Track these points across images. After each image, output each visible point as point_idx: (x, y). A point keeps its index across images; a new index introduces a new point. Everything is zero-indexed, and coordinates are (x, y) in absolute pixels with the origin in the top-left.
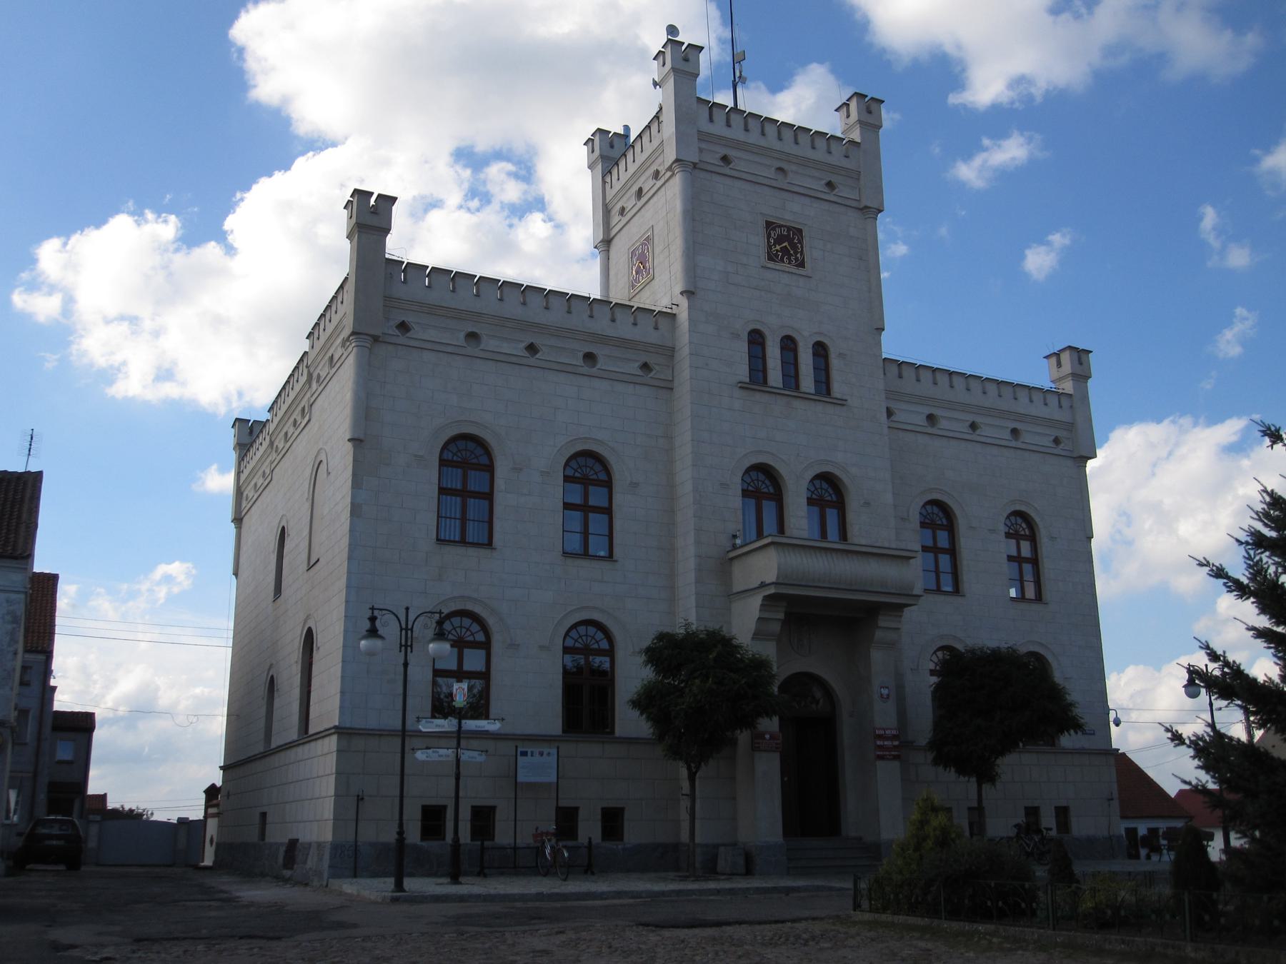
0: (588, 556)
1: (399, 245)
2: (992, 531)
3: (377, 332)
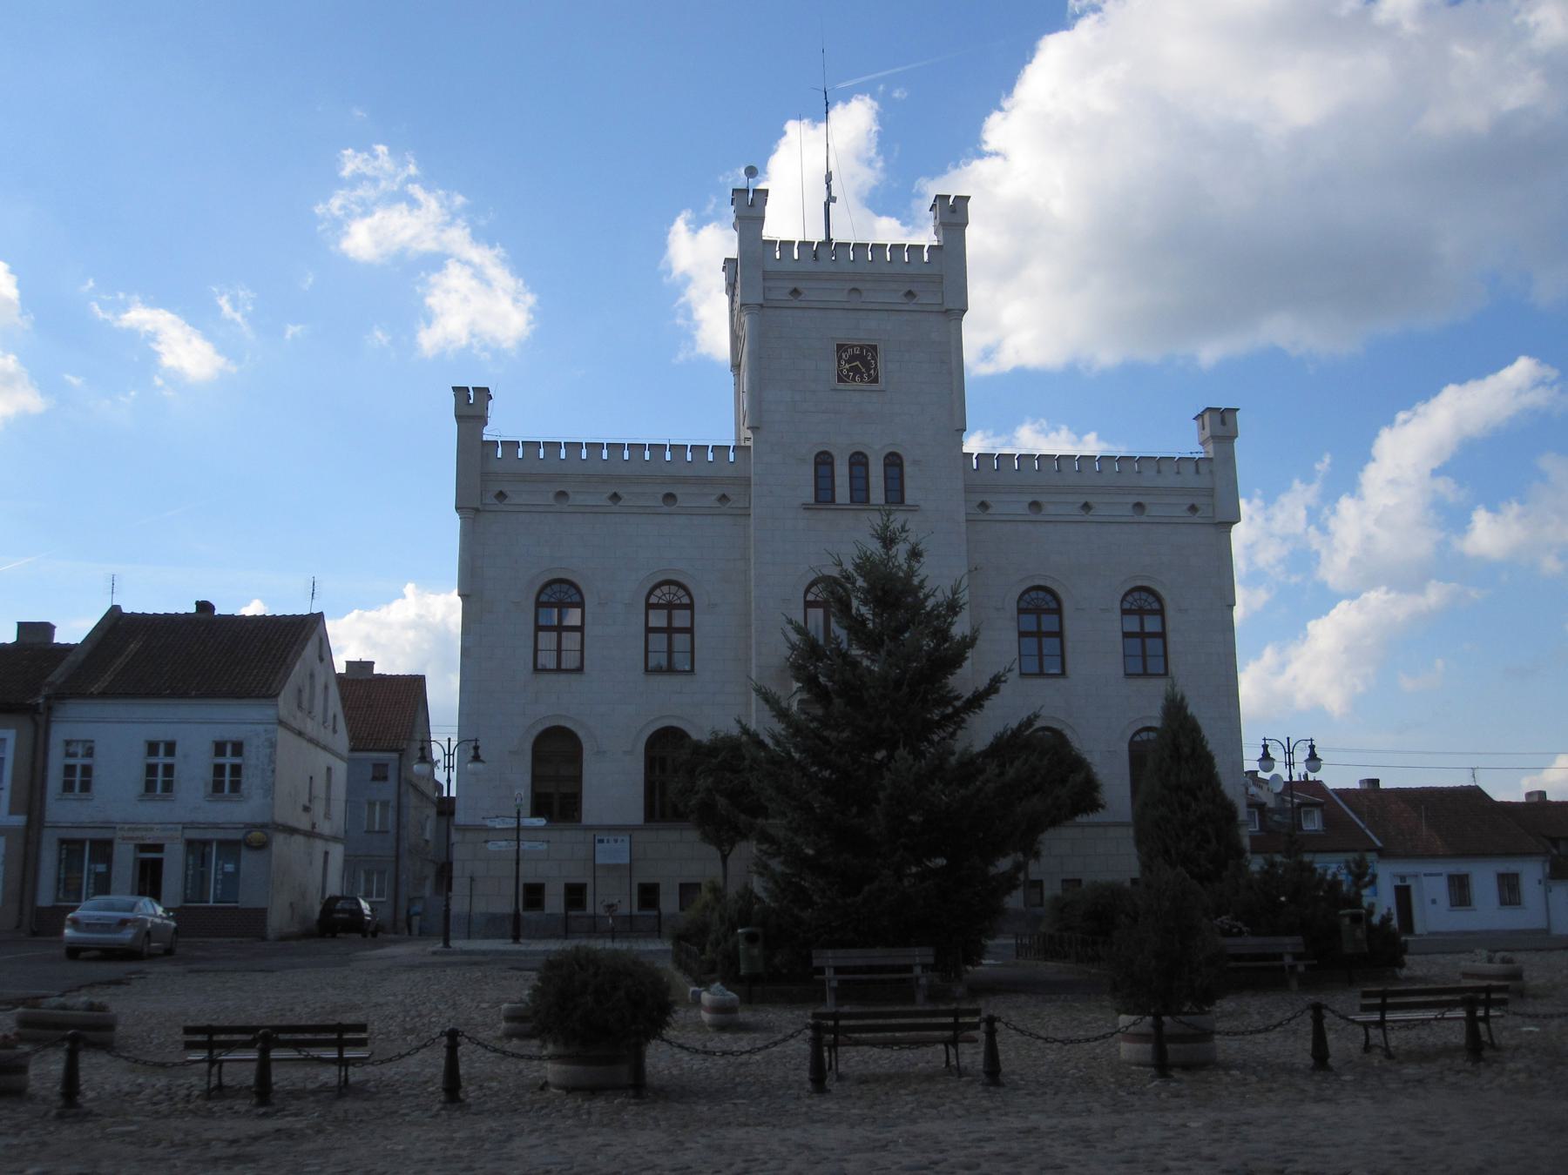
0: (1044, 674)
1: (497, 428)
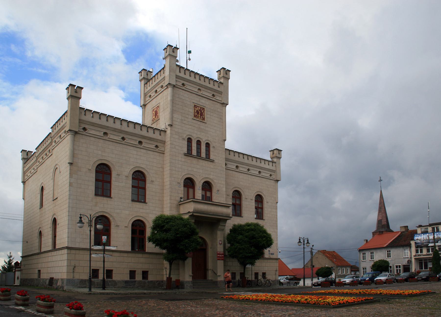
2: (252, 200)
3: (77, 130)
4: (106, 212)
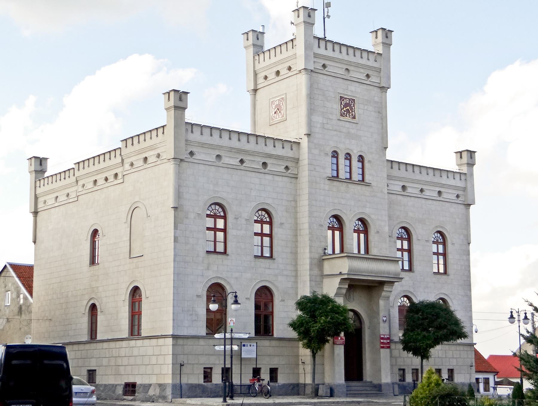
4: (221, 278)
